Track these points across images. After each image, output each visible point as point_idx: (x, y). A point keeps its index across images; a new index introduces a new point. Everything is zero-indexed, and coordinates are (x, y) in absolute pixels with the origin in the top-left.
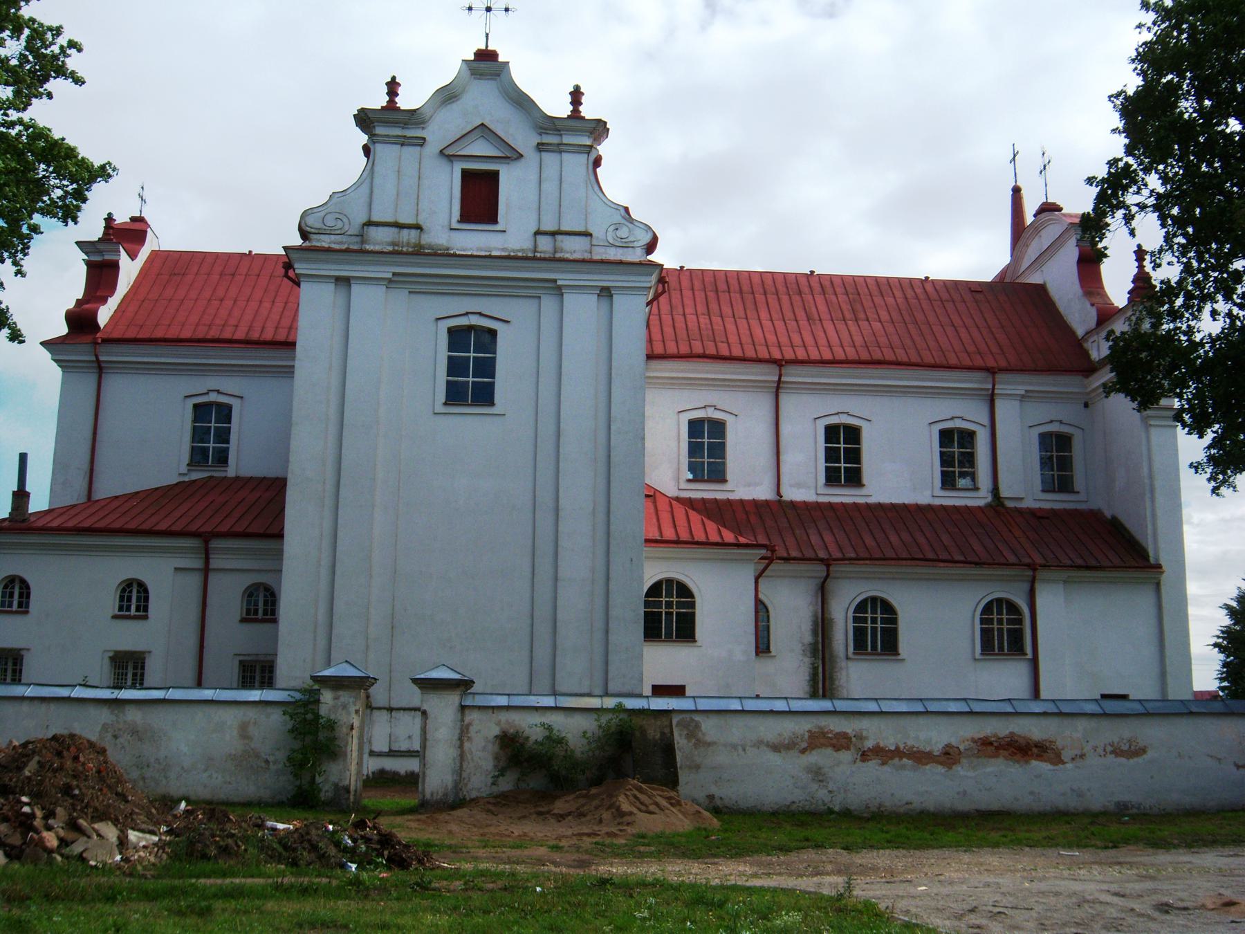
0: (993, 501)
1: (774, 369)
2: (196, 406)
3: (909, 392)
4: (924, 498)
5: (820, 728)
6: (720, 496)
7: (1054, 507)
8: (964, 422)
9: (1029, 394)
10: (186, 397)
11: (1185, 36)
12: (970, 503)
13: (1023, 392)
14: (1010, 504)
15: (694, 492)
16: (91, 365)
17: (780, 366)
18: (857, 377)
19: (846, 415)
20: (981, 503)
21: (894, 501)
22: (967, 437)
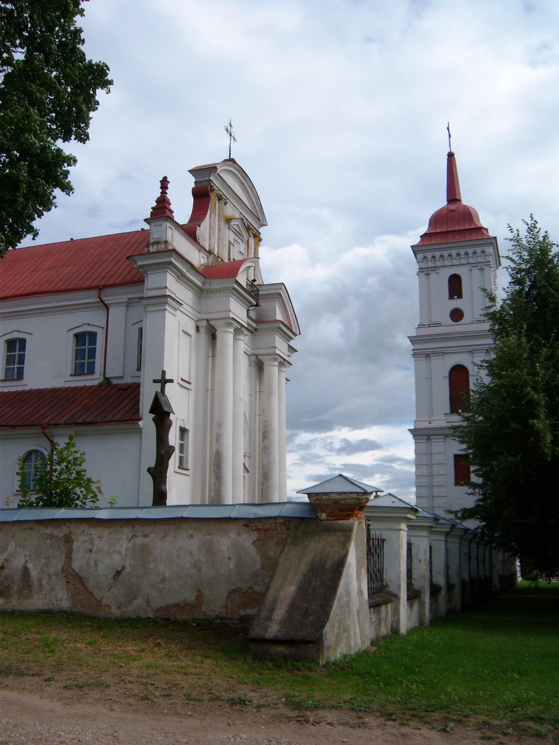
0: (104, 380)
1: (96, 292)
2: (76, 336)
3: (36, 313)
4: (59, 383)
5: (349, 627)
6: (20, 389)
7: (71, 386)
8: (20, 333)
9: (131, 301)
10: (68, 331)
11: (21, 126)
12: (89, 384)
13: (126, 300)
14: (114, 382)
15: (72, 382)
16: (98, 305)
17: (100, 289)
18: (17, 306)
19: (17, 332)
20: (96, 383)
21: (42, 387)
22: (93, 336)
